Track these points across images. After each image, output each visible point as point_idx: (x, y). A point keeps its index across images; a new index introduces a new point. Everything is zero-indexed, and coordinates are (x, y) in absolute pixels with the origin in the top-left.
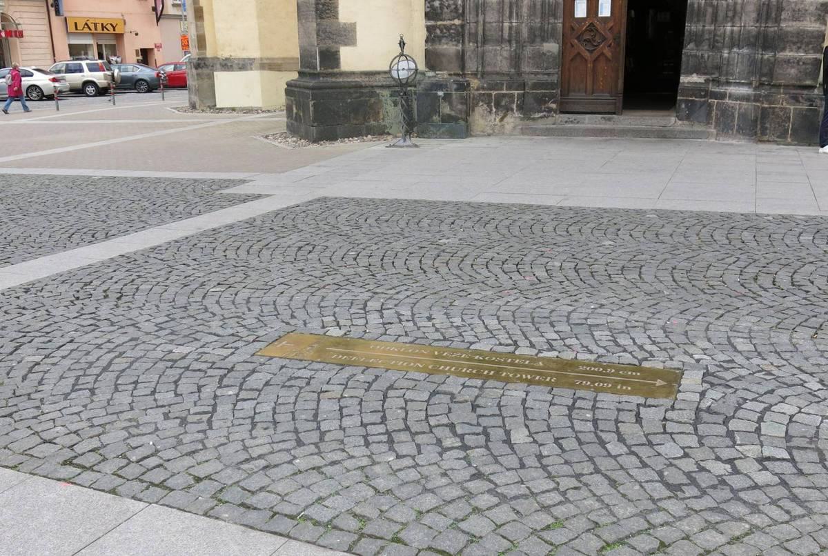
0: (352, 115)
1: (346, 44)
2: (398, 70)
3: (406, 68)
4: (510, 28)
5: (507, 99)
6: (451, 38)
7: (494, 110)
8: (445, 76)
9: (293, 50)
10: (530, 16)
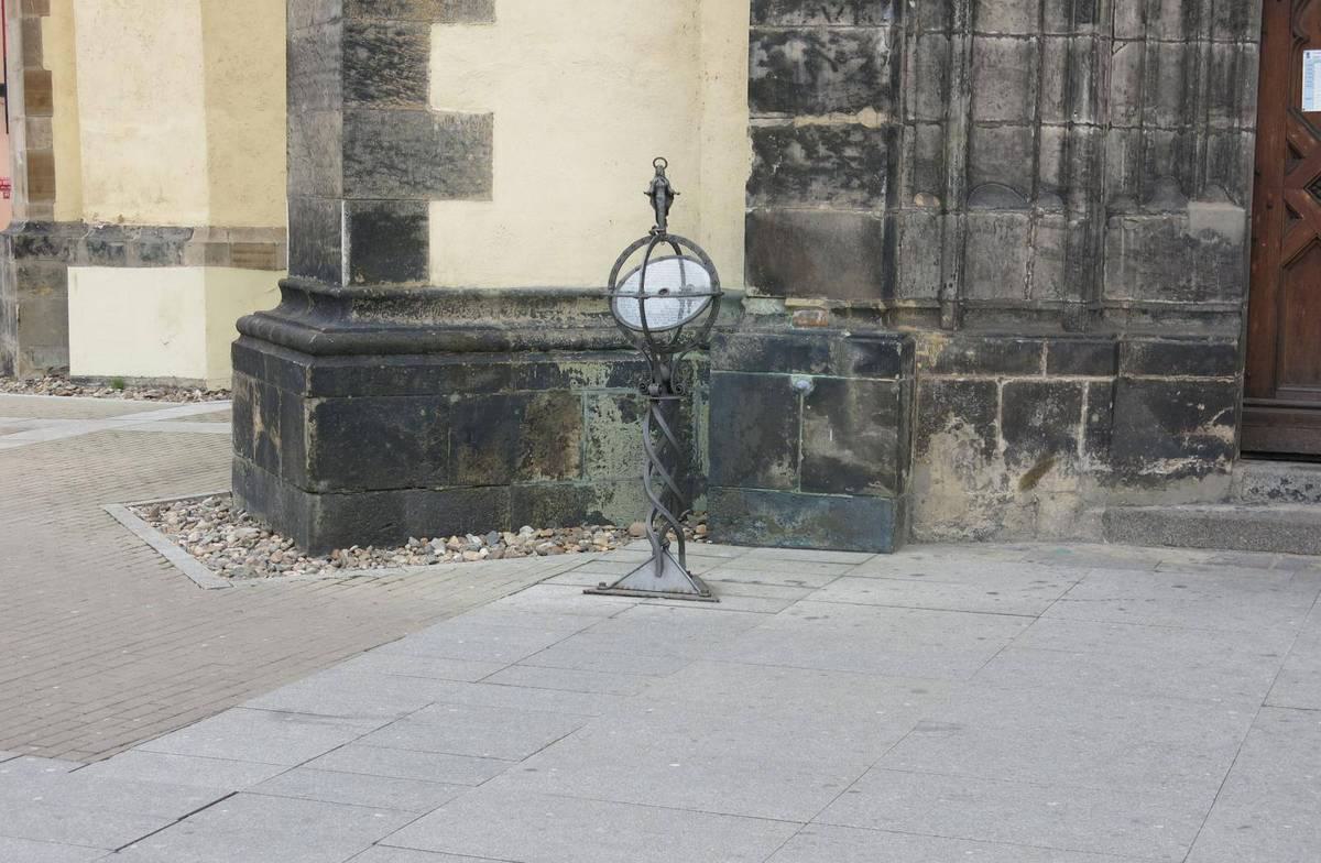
0: (464, 452)
1: (452, 193)
2: (642, 297)
3: (675, 287)
4: (1067, 145)
5: (1051, 405)
6: (845, 175)
7: (1002, 444)
8: (820, 317)
9: (270, 212)
10: (1137, 102)
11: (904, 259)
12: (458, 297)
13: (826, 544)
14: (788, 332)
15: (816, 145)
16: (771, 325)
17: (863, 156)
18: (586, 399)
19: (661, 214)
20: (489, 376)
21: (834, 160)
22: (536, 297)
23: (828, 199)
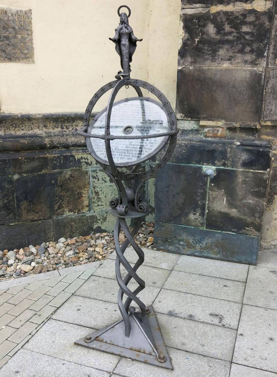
0: (24, 204)
6: (241, 45)
11: (267, 98)
12: (18, 119)
13: (219, 256)
14: (201, 141)
15: (224, 25)
16: (190, 136)
17: (254, 31)
18: (90, 172)
19: (126, 60)
20: (36, 164)
21: (234, 34)
22: (63, 118)
23: (229, 60)
